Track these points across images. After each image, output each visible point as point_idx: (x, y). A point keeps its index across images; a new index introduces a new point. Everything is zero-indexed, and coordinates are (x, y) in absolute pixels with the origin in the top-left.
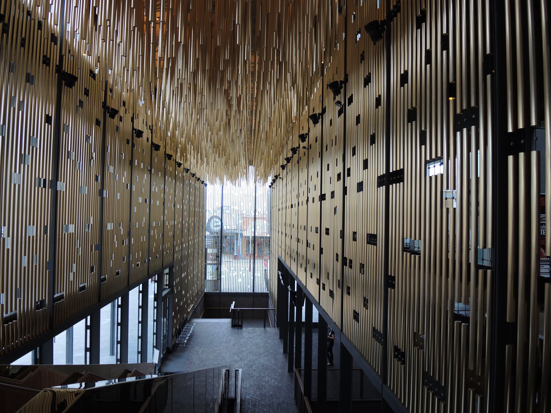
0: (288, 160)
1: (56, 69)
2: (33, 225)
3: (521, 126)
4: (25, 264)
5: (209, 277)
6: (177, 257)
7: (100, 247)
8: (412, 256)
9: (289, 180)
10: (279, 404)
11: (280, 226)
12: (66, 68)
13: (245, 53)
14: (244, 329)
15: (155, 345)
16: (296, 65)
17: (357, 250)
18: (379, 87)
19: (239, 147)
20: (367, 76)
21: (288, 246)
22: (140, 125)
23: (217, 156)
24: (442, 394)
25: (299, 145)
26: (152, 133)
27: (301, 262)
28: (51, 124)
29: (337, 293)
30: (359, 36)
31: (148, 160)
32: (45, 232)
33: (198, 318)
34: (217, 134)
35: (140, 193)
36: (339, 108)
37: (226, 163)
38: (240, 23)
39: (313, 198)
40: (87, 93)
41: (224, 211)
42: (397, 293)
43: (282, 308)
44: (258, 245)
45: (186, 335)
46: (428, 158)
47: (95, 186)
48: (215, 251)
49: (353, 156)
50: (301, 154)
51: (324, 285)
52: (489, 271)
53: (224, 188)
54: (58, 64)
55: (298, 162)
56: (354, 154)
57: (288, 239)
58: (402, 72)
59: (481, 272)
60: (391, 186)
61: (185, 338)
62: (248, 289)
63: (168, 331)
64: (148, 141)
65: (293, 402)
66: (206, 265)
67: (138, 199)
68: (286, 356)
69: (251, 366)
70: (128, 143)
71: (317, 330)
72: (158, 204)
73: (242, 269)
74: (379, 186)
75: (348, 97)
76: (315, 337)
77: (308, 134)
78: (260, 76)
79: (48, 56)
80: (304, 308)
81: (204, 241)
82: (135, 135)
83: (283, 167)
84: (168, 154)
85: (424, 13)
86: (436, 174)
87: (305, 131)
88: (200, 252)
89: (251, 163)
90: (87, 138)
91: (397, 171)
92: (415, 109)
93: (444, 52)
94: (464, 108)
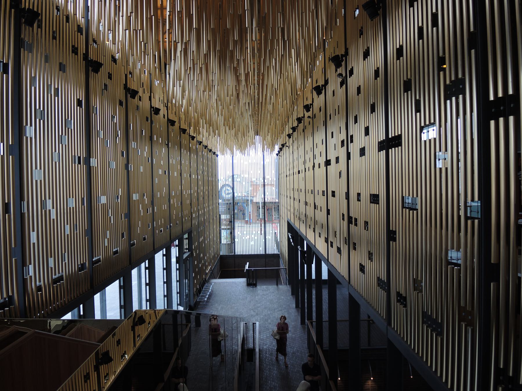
0: (294, 129)
1: (83, 57)
2: (73, 197)
3: (500, 95)
4: (68, 232)
5: (224, 241)
6: (195, 224)
8: (411, 212)
9: (295, 147)
10: (293, 353)
11: (288, 191)
13: (253, 36)
14: (258, 287)
15: (179, 303)
16: (299, 39)
17: (361, 210)
19: (248, 120)
20: (366, 50)
22: (157, 104)
23: (227, 128)
25: (304, 114)
26: (167, 110)
27: (309, 224)
29: (344, 250)
30: (357, 12)
31: (165, 134)
32: (83, 203)
34: (228, 108)
35: (162, 166)
36: (341, 79)
37: (236, 135)
38: (249, 8)
39: (319, 164)
40: (110, 77)
41: (235, 180)
42: (398, 245)
44: (268, 210)
46: (423, 125)
47: (122, 161)
48: (228, 217)
49: (355, 124)
50: (306, 124)
51: (332, 243)
52: (476, 221)
53: (234, 158)
54: (84, 52)
55: (304, 131)
56: (356, 122)
57: (296, 203)
58: (398, 47)
59: (469, 222)
60: (390, 150)
61: (205, 297)
63: (189, 290)
64: (164, 117)
65: (306, 351)
66: (220, 230)
68: (298, 311)
69: (267, 320)
70: (147, 120)
71: (327, 286)
72: (176, 175)
73: (254, 232)
74: (380, 150)
75: (349, 69)
76: (325, 293)
77: (312, 104)
78: (264, 50)
79: (76, 46)
80: (313, 266)
81: (217, 208)
83: (289, 136)
86: (430, 138)
87: (309, 102)
88: (215, 218)
89: (257, 133)
90: (113, 117)
91: (395, 136)
92: (410, 80)
93: (435, 29)
94: (453, 79)
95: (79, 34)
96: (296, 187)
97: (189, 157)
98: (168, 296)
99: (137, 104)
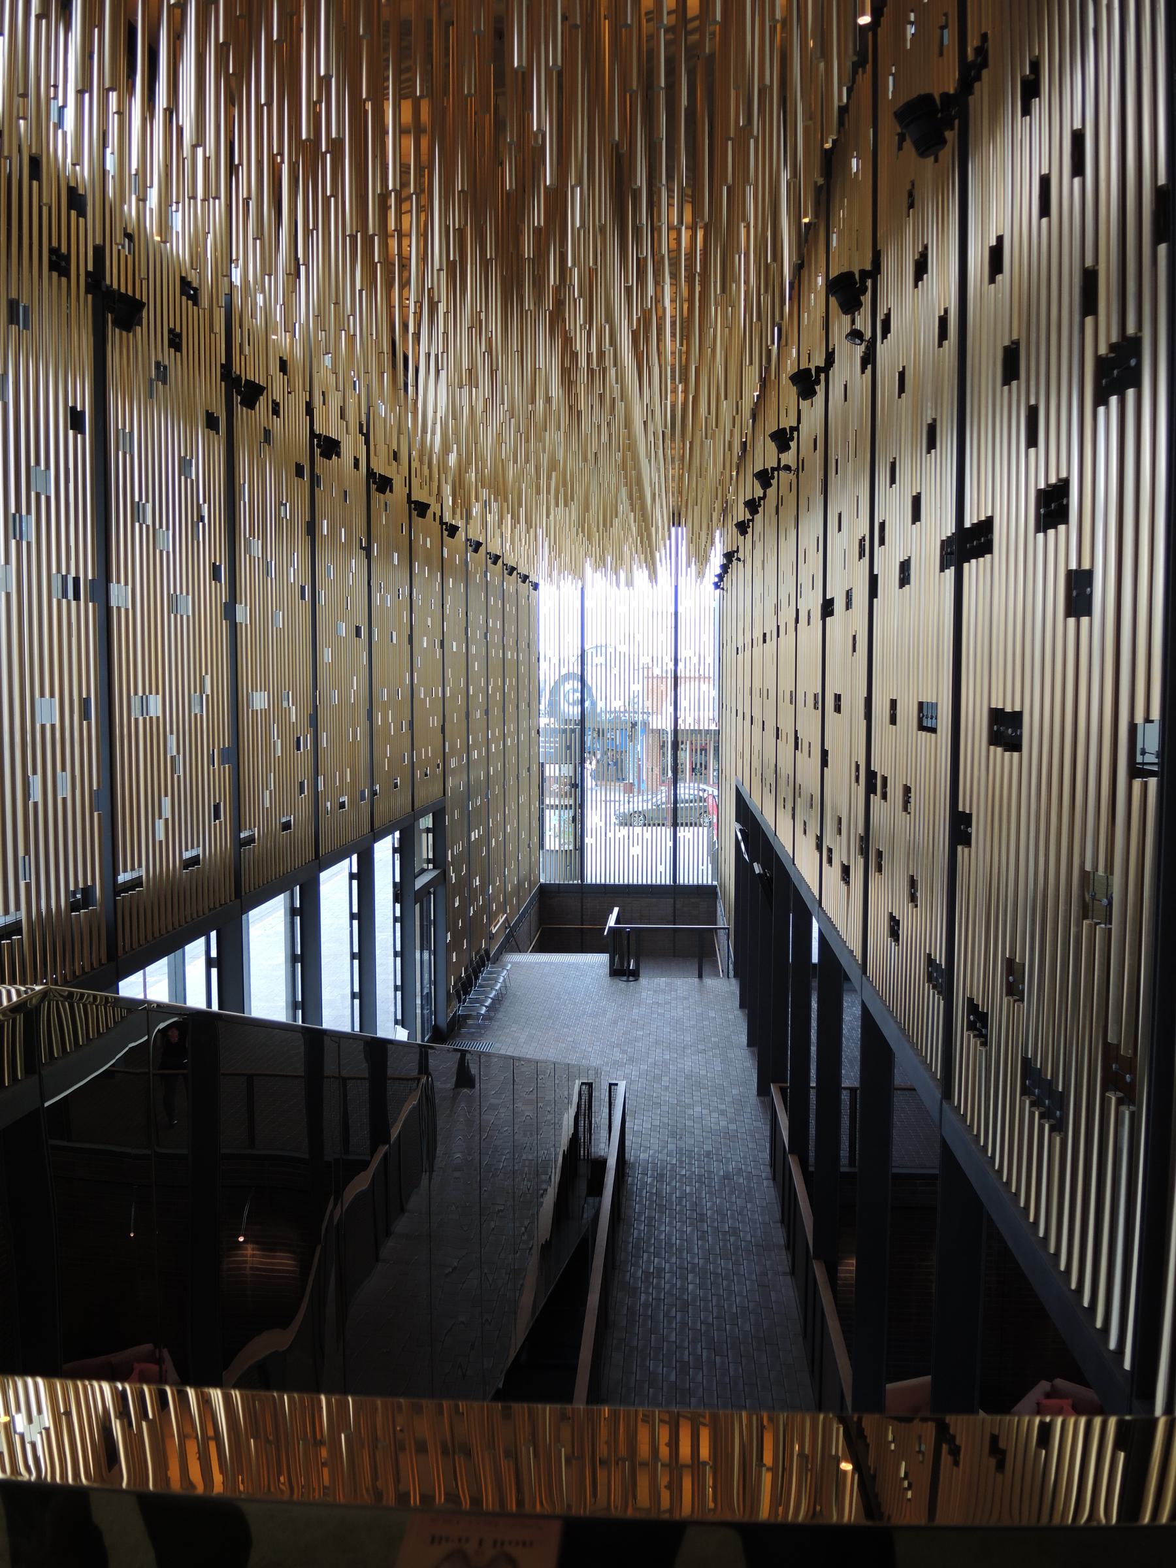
1: (1139, 356)
2: (52, 695)
5: (551, 843)
7: (233, 755)
10: (726, 1177)
12: (113, 279)
14: (643, 981)
15: (399, 1017)
18: (941, 287)
21: (756, 752)
22: (328, 425)
24: (1058, 1113)
26: (367, 443)
28: (83, 433)
32: (85, 715)
33: (520, 950)
37: (582, 525)
40: (175, 341)
42: (973, 858)
43: (754, 930)
45: (486, 994)
47: (214, 594)
48: (567, 770)
51: (830, 850)
54: (90, 268)
60: (966, 565)
61: (482, 1003)
62: (661, 876)
64: (356, 466)
65: (766, 1172)
67: (336, 629)
69: (658, 1079)
77: (797, 429)
79: (64, 250)
82: (317, 451)
84: (416, 502)
85: (1036, 66)
87: (788, 422)
88: (524, 774)
89: (676, 519)
90: (185, 465)
95: (73, 213)
96: (757, 685)
97: (437, 588)
98: (365, 995)
99: (264, 423)
